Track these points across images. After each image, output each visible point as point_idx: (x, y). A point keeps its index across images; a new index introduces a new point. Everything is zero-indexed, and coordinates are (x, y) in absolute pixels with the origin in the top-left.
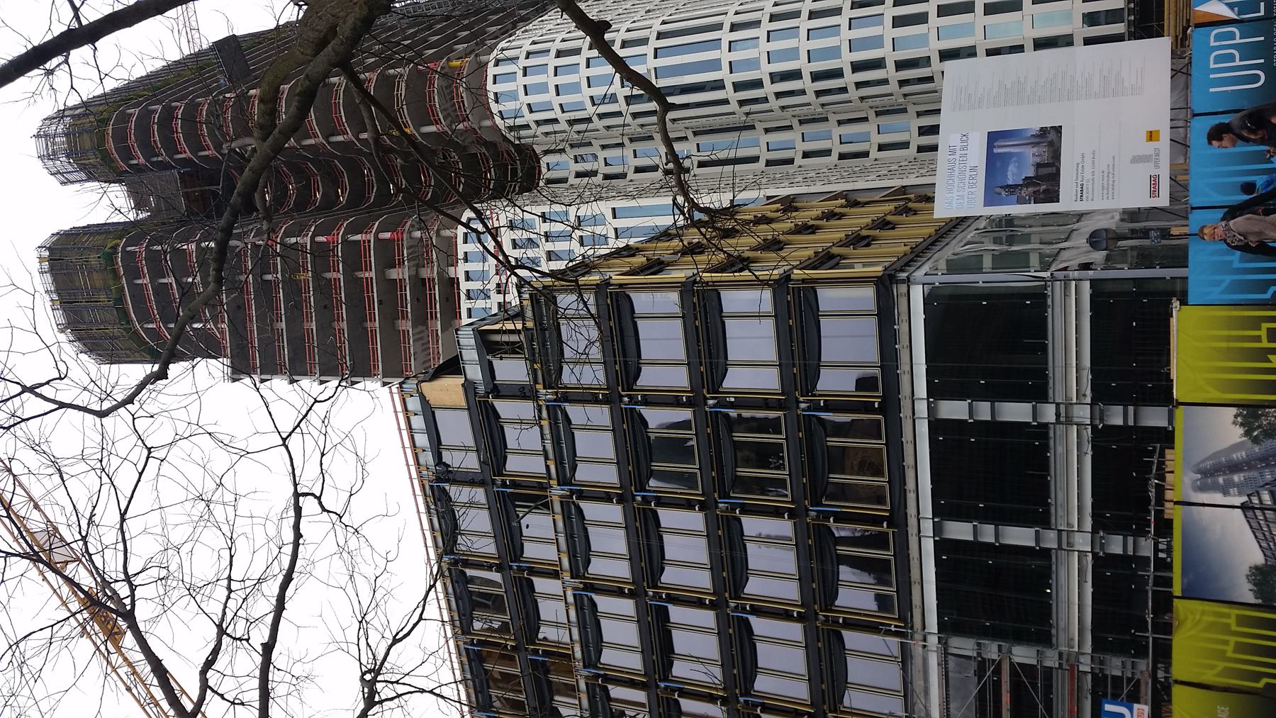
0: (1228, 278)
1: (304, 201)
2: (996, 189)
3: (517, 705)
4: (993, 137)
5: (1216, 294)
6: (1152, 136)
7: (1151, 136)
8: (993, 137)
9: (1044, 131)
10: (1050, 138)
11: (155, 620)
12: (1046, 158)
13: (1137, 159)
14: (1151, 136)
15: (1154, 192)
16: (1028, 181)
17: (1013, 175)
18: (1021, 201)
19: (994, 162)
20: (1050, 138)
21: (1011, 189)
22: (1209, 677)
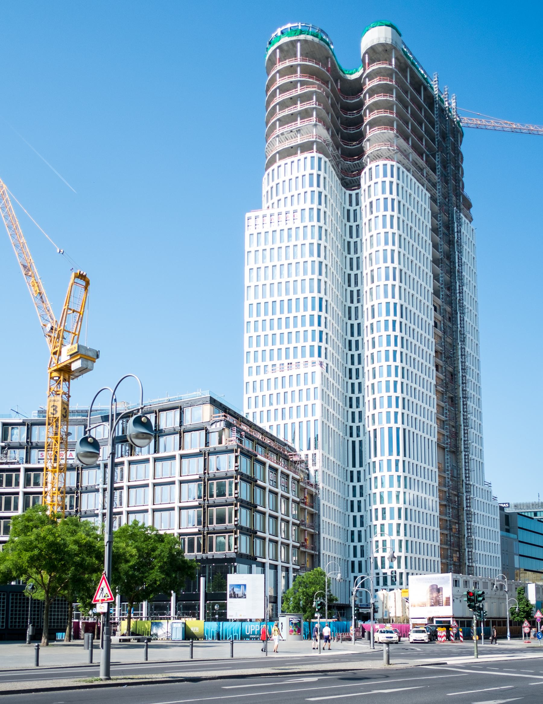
0: (209, 629)
1: (38, 604)
2: (233, 586)
3: (2, 626)
4: (245, 586)
5: (206, 627)
6: (241, 615)
7: (507, 523)
8: (245, 586)
9: (245, 595)
10: (244, 596)
11: (377, 157)
12: (239, 596)
13: (236, 613)
14: (507, 523)
15: (230, 616)
16: (234, 593)
17: (236, 590)
18: (230, 591)
19: (239, 586)
20: (244, 596)
21: (233, 589)
22: (138, 627)
